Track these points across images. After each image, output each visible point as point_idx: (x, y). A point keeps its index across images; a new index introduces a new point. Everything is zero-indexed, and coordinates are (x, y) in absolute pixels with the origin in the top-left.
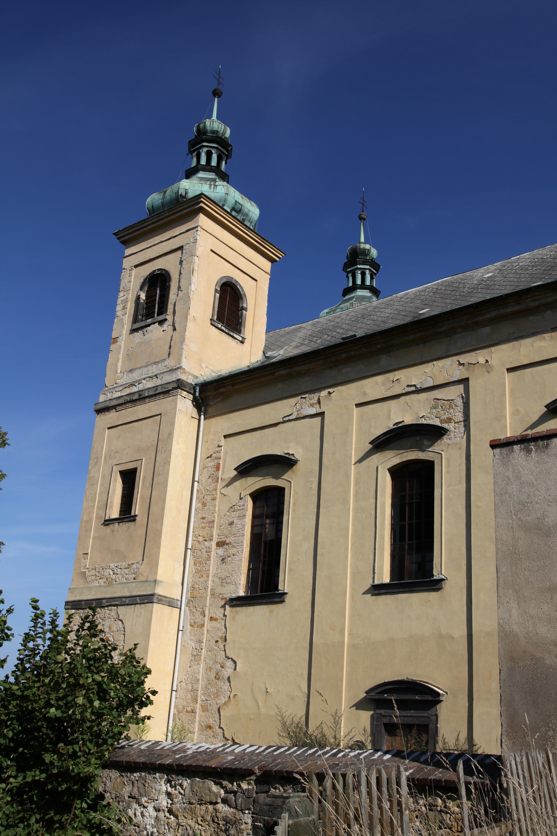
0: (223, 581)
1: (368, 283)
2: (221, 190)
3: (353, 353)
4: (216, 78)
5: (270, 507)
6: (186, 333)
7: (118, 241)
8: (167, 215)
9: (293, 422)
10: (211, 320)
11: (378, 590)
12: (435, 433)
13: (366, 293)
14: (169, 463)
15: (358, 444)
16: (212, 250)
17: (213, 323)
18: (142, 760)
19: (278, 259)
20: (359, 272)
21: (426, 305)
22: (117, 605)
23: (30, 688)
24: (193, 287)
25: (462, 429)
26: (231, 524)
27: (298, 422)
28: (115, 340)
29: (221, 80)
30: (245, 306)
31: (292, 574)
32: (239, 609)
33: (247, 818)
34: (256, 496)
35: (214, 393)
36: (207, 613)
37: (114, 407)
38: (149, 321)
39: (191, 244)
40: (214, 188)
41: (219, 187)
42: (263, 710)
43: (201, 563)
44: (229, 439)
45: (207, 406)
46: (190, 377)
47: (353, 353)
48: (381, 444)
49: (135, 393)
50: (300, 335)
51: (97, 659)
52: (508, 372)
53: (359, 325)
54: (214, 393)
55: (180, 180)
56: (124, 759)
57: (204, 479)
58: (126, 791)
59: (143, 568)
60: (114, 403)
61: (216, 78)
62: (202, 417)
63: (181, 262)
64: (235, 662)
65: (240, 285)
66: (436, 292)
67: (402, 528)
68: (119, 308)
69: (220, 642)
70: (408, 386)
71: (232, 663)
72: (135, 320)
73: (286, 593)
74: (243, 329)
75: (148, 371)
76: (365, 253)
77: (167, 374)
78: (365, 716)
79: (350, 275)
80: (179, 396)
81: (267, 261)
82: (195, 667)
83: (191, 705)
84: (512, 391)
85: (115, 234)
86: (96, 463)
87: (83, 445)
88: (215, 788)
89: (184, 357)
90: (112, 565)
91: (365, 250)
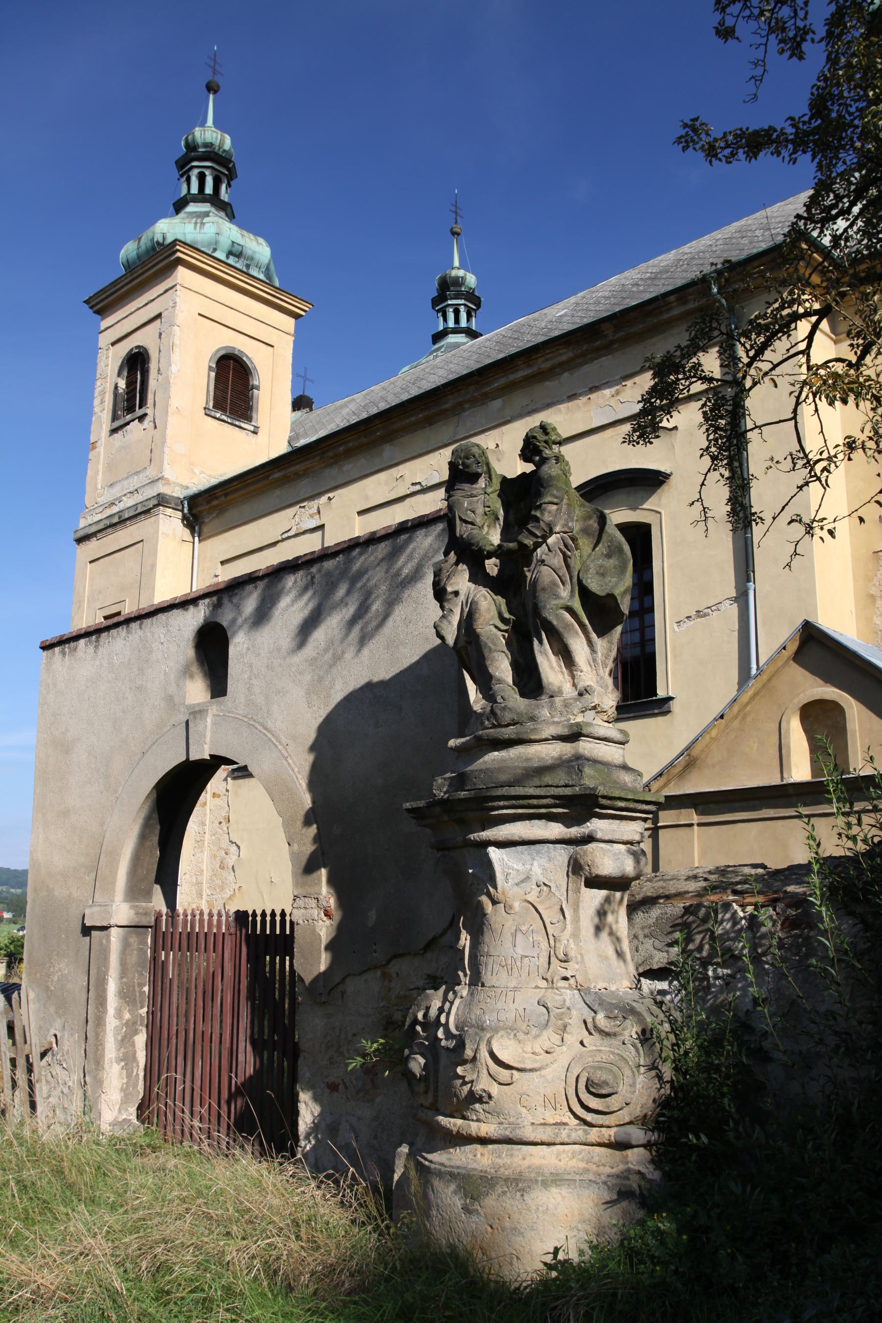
3: (351, 444)
4: (210, 66)
6: (168, 432)
7: (91, 311)
8: (141, 271)
9: (293, 539)
10: (205, 408)
13: (461, 338)
16: (199, 314)
17: (208, 412)
19: (303, 313)
20: (451, 310)
24: (174, 368)
27: (298, 538)
28: (94, 445)
29: (217, 67)
30: (256, 383)
35: (207, 507)
37: (94, 534)
39: (170, 310)
40: (200, 228)
41: (207, 225)
44: (226, 566)
45: (201, 524)
46: (177, 488)
47: (351, 444)
49: (115, 514)
54: (207, 507)
60: (94, 529)
61: (210, 66)
62: (197, 539)
64: (239, 847)
65: (247, 357)
68: (96, 402)
69: (223, 824)
70: (413, 484)
71: (236, 848)
72: (115, 418)
74: (254, 415)
75: (129, 484)
76: (458, 282)
77: (146, 487)
79: (440, 314)
80: (161, 515)
81: (288, 317)
82: (198, 855)
83: (196, 901)
85: (85, 302)
86: (79, 608)
89: (166, 463)
91: (458, 278)
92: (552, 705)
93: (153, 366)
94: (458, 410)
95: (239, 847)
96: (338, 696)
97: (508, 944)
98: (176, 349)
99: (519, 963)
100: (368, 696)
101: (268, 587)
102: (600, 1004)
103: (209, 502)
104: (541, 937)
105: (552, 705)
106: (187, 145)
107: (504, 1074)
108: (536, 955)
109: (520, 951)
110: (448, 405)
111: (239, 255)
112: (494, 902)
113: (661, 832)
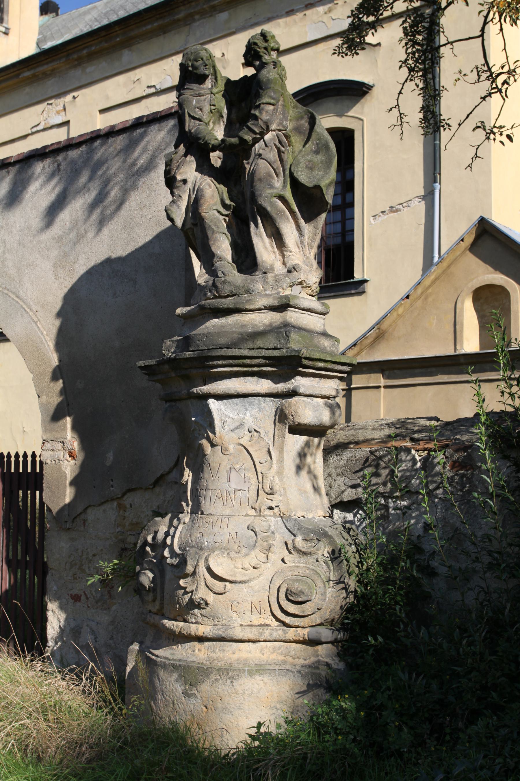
9: (42, 134)
47: (93, 48)
52: (243, 67)
73: (366, 281)
74: (5, 17)
92: (265, 281)
99: (232, 496)
100: (108, 270)
102: (298, 529)
105: (265, 281)
107: (218, 586)
108: (247, 489)
110: (181, 16)
112: (213, 445)
113: (354, 393)
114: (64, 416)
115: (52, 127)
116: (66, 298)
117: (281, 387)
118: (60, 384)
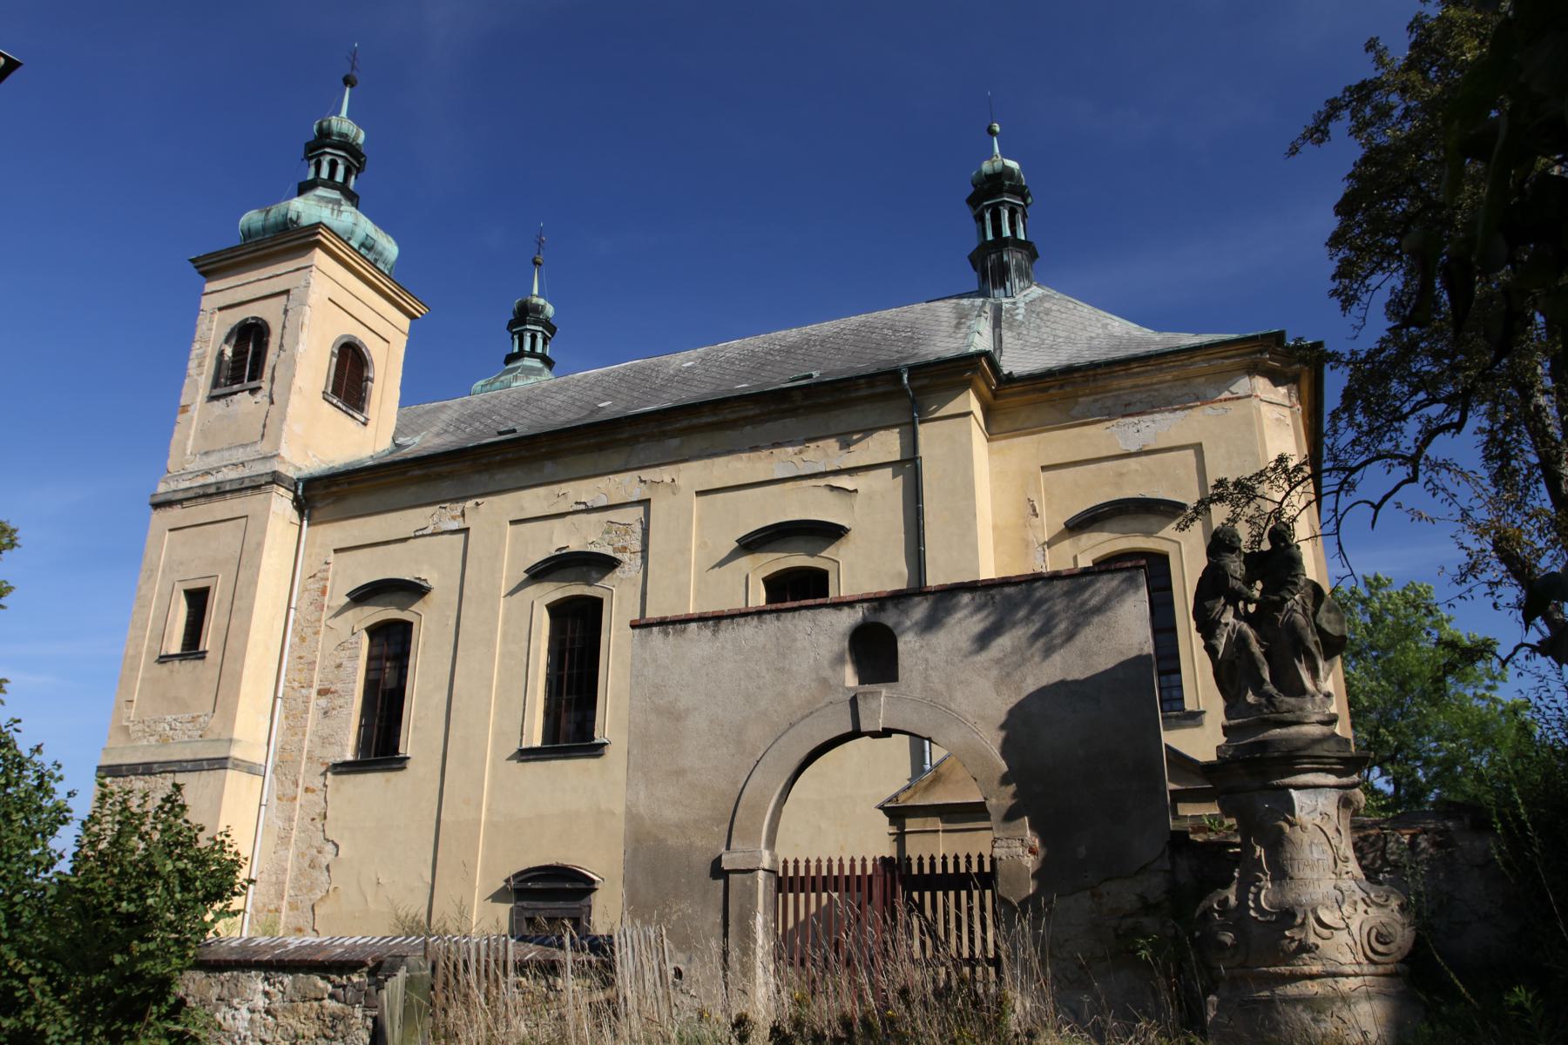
0: (325, 741)
1: (539, 350)
2: (349, 219)
5: (392, 644)
11: (526, 755)
12: (606, 564)
13: (536, 363)
14: (256, 583)
15: (510, 570)
18: (234, 957)
21: (608, 396)
22: (174, 772)
23: (93, 880)
24: (301, 348)
25: (639, 561)
26: (339, 666)
28: (185, 409)
31: (418, 731)
32: (345, 777)
33: (358, 1012)
34: (375, 631)
36: (301, 782)
37: (180, 502)
38: (236, 387)
42: (372, 906)
43: (295, 719)
45: (312, 508)
48: (540, 573)
50: (444, 417)
51: (180, 841)
53: (522, 413)
55: (290, 197)
56: (212, 957)
57: (304, 605)
58: (213, 993)
59: (215, 723)
63: (286, 311)
64: (337, 846)
66: (622, 378)
67: (560, 680)
68: (192, 364)
76: (538, 309)
78: (504, 910)
84: (700, 519)
85: (192, 261)
87: (131, 555)
88: (321, 983)
90: (169, 718)
92: (1314, 702)
93: (274, 341)
94: (633, 441)
95: (337, 846)
96: (1030, 686)
97: (1307, 851)
98: (305, 329)
100: (1061, 691)
101: (936, 602)
103: (327, 487)
104: (1327, 847)
105: (1314, 702)
106: (320, 129)
107: (1325, 932)
109: (1316, 856)
110: (625, 435)
111: (370, 249)
112: (1292, 825)
114: (1022, 816)
115: (442, 533)
116: (1011, 713)
117: (1345, 780)
118: (1012, 788)
